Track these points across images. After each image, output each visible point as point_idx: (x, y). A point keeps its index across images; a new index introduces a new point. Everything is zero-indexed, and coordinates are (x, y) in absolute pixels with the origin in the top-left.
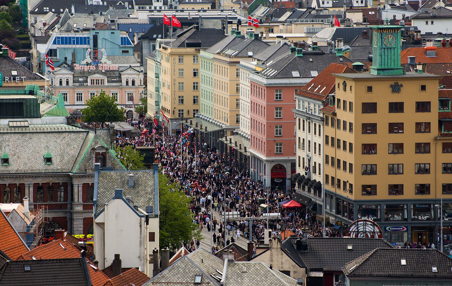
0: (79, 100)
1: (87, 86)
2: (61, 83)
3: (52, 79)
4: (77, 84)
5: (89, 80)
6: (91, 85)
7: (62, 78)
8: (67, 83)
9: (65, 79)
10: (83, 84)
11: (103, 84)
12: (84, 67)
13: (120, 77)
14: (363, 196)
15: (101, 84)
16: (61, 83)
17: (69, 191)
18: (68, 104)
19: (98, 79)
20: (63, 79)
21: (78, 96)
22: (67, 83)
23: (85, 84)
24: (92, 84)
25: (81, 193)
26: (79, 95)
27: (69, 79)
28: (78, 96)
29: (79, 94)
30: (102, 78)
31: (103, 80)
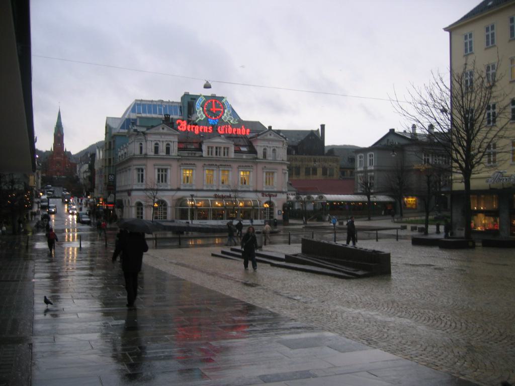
0: (162, 181)
1: (202, 156)
2: (156, 150)
3: (141, 144)
4: (185, 153)
5: (204, 147)
6: (207, 156)
7: (158, 142)
8: (168, 150)
9: (165, 144)
10: (195, 154)
11: (227, 155)
12: (194, 128)
13: (200, 144)
14: (418, 249)
15: (216, 154)
16: (156, 150)
17: (239, 317)
18: (169, 188)
19: (219, 145)
20: (160, 144)
21: (161, 173)
22: (168, 150)
23: (198, 154)
24: (208, 154)
25: (342, 266)
26: (162, 171)
27: (171, 144)
28: (161, 173)
29: (162, 170)
30: (226, 146)
31: (228, 148)
